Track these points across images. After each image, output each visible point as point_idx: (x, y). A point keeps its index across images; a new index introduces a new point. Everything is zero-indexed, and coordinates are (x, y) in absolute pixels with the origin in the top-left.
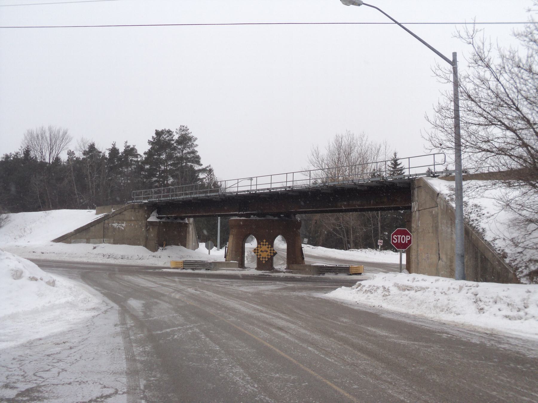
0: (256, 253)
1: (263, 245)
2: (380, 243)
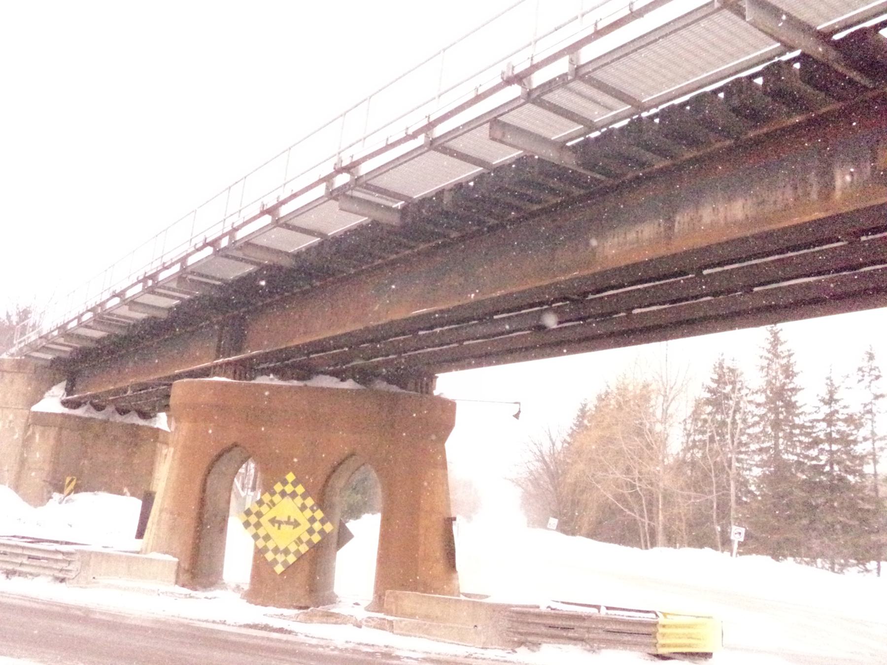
0: (252, 529)
1: (283, 494)
2: (737, 536)
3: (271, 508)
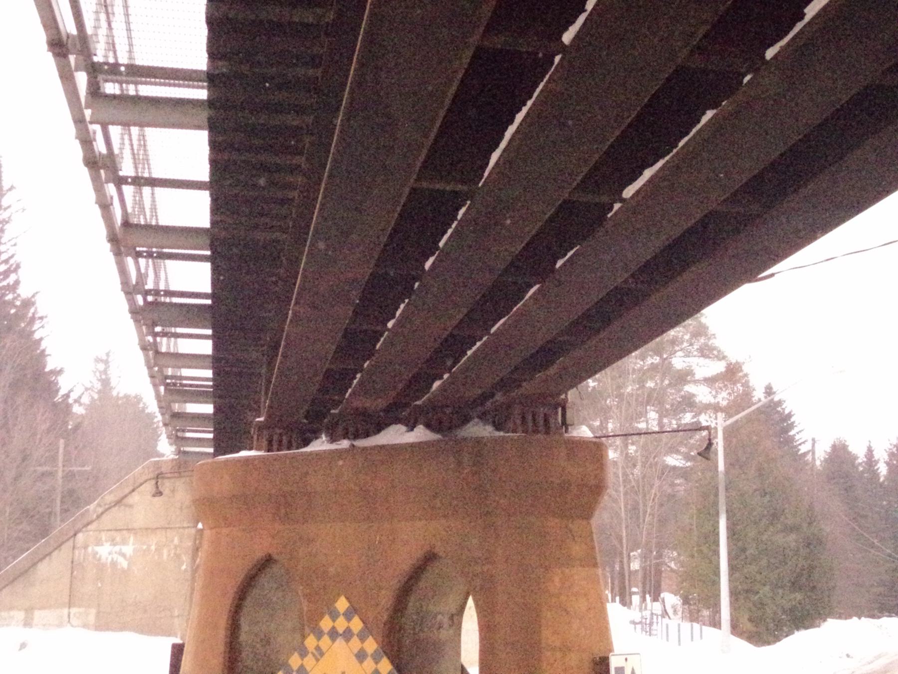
1: (333, 634)
3: (317, 660)
